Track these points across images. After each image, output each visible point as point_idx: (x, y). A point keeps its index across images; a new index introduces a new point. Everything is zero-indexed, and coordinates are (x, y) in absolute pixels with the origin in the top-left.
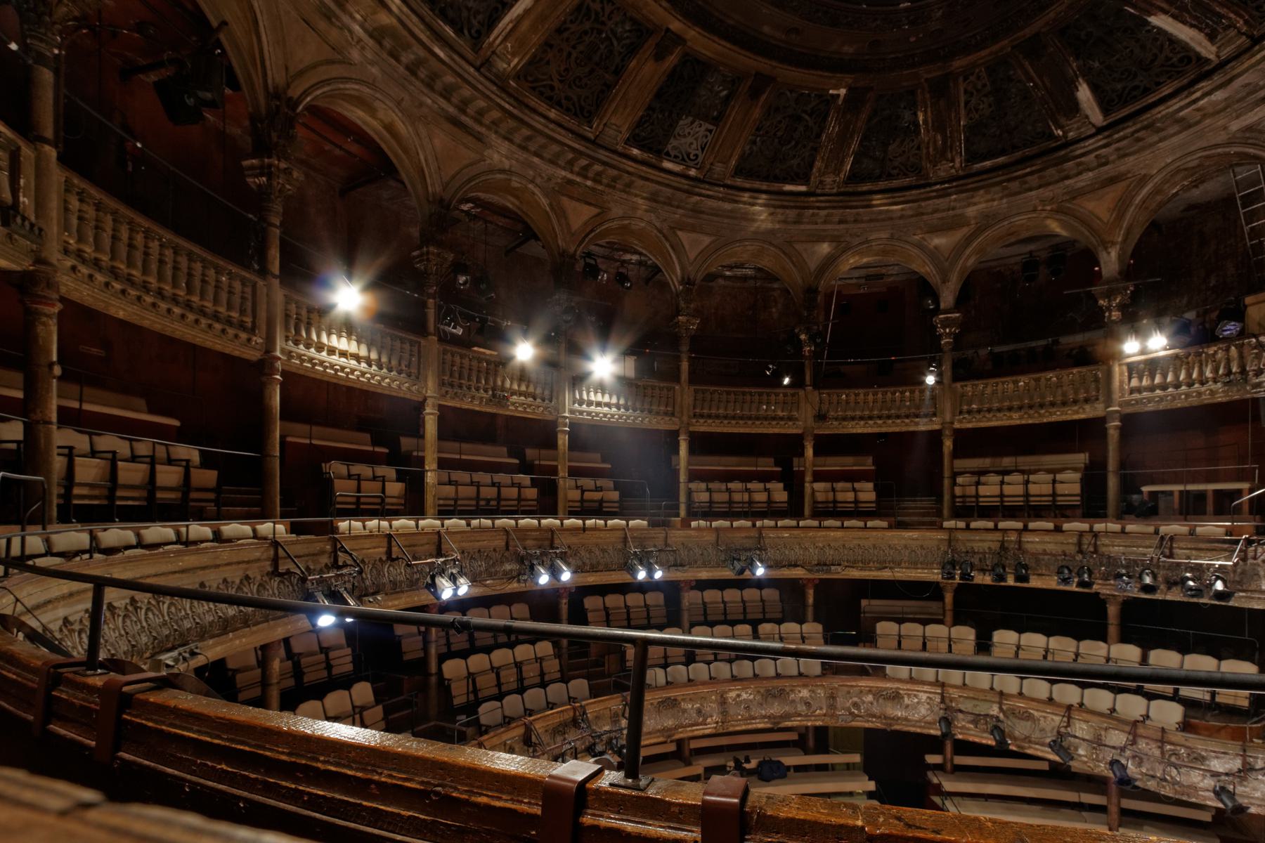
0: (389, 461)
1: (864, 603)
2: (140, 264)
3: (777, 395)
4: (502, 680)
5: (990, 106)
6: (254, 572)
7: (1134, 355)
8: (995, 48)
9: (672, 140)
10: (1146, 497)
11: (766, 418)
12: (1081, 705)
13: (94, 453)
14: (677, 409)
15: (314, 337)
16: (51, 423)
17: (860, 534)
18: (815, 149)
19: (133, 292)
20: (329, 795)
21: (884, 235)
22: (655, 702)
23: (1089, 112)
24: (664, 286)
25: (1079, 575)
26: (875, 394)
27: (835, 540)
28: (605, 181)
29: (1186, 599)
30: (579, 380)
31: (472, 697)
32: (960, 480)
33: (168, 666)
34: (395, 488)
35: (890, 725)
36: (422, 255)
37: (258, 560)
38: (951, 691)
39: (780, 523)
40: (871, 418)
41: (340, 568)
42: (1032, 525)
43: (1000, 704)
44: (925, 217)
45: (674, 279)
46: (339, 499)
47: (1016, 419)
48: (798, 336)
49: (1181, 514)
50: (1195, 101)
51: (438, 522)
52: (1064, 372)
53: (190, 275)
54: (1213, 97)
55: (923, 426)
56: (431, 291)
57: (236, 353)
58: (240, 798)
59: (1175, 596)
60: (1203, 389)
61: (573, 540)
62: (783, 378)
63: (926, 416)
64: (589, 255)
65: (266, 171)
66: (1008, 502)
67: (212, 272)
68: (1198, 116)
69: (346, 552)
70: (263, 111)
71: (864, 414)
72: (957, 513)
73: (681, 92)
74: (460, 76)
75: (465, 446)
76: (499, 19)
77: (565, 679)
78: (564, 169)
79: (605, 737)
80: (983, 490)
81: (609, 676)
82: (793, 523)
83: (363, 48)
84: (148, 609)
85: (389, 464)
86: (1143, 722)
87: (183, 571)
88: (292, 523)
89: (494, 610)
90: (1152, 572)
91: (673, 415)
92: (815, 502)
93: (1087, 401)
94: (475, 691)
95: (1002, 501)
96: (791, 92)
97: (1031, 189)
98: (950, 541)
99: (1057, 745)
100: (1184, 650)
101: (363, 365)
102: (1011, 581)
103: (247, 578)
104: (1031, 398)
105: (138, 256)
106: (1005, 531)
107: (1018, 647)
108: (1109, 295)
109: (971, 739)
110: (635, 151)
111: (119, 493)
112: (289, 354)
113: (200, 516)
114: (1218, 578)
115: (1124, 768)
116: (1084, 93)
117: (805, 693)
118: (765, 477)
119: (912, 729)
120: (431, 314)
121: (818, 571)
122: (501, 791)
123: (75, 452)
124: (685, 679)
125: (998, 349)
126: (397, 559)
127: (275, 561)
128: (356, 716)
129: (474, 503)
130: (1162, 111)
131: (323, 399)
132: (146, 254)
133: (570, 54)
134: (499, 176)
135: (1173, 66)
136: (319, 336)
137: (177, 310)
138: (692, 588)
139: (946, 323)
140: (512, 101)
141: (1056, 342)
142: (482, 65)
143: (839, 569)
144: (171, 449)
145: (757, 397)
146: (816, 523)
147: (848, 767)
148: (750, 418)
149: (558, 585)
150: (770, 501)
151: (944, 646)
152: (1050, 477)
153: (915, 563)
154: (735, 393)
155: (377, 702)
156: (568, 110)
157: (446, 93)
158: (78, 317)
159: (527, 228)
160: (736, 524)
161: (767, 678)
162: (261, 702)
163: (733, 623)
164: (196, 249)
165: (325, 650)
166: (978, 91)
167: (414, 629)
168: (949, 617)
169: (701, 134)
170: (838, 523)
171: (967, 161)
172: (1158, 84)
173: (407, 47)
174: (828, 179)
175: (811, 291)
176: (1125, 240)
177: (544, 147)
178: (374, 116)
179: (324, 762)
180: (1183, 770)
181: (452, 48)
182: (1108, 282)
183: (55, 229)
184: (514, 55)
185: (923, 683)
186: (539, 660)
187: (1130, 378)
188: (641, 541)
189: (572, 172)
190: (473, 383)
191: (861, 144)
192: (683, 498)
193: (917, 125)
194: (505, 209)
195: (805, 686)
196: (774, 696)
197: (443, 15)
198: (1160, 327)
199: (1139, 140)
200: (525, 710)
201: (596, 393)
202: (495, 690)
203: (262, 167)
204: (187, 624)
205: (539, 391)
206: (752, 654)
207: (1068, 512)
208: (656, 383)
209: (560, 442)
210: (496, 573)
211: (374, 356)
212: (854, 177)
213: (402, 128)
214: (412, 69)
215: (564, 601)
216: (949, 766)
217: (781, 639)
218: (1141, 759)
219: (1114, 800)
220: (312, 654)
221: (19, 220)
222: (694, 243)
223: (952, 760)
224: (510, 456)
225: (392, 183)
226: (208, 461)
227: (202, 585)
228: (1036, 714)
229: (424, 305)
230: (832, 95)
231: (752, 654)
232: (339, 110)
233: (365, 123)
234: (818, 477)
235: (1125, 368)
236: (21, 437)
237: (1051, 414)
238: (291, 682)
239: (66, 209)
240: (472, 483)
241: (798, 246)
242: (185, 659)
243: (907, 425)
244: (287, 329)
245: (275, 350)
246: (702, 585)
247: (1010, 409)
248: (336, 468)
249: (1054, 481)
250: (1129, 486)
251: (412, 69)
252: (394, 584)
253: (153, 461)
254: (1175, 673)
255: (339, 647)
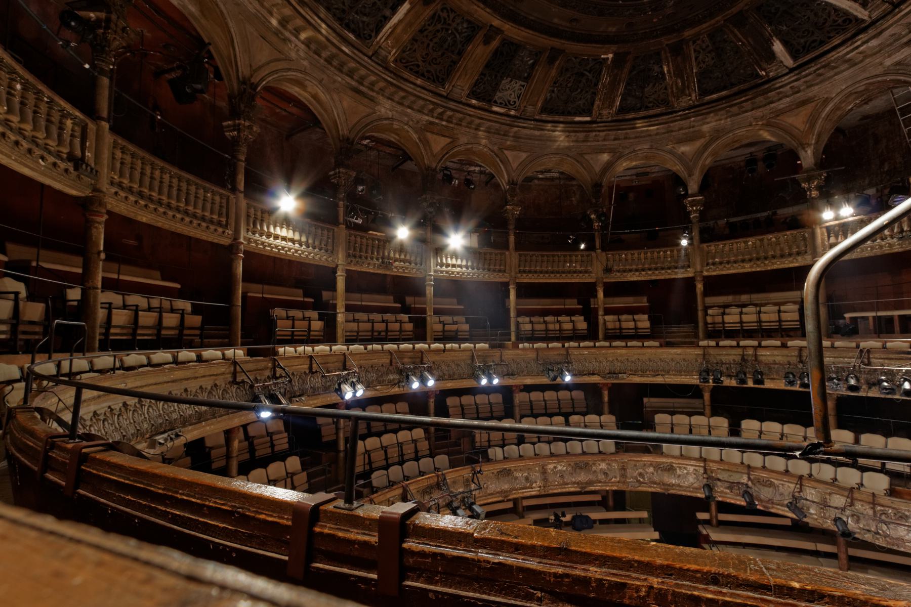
0: (314, 307)
1: (645, 400)
2: (157, 188)
3: (576, 256)
4: (389, 456)
5: (713, 59)
6: (220, 382)
7: (830, 221)
8: (713, 21)
9: (498, 93)
10: (848, 321)
11: (569, 272)
12: (810, 475)
13: (125, 307)
14: (507, 268)
15: (265, 229)
16: (97, 288)
17: (639, 351)
18: (594, 93)
19: (152, 206)
20: (182, 514)
21: (646, 146)
22: (495, 472)
23: (783, 59)
24: (497, 186)
25: (801, 378)
26: (646, 253)
27: (621, 355)
28: (454, 121)
29: (883, 396)
30: (439, 250)
31: (367, 467)
32: (710, 312)
33: (160, 443)
34: (317, 325)
35: (668, 490)
36: (335, 174)
37: (223, 374)
38: (711, 464)
39: (582, 344)
40: (643, 270)
41: (277, 378)
42: (764, 343)
43: (749, 474)
44: (674, 134)
45: (503, 182)
46: (278, 333)
47: (747, 268)
48: (589, 216)
49: (875, 333)
50: (857, 48)
51: (345, 347)
52: (780, 234)
53: (188, 194)
54: (870, 44)
55: (680, 274)
56: (341, 196)
57: (216, 241)
58: (136, 517)
59: (874, 393)
60: (883, 243)
61: (437, 358)
62: (579, 244)
63: (683, 267)
64: (446, 168)
65: (237, 128)
66: (746, 326)
67: (201, 191)
68: (861, 57)
69: (281, 368)
70: (236, 92)
71: (637, 267)
72: (710, 335)
73: (503, 62)
74: (359, 63)
75: (364, 296)
76: (382, 27)
77: (432, 455)
78: (427, 115)
79: (459, 497)
80: (727, 318)
81: (463, 453)
82: (591, 344)
83: (298, 50)
84: (149, 406)
85: (314, 309)
86: (859, 489)
87: (173, 381)
88: (248, 349)
89: (385, 406)
90: (856, 377)
91: (505, 271)
92: (607, 329)
93: (798, 254)
94: (370, 463)
95: (742, 326)
96: (576, 58)
97: (746, 112)
98: (704, 355)
99: (792, 506)
100: (887, 434)
101: (297, 245)
102: (750, 384)
103: (216, 385)
104: (758, 253)
105: (156, 184)
106: (745, 347)
107: (761, 432)
108: (809, 180)
109: (728, 501)
110: (474, 102)
111: (139, 332)
112: (249, 240)
113: (190, 345)
114: (905, 380)
115: (846, 524)
116: (778, 47)
117: (603, 466)
118: (570, 313)
119: (684, 493)
120: (341, 211)
121: (610, 378)
122: (273, 511)
123: (113, 306)
124: (517, 455)
125: (732, 220)
126: (316, 372)
127: (234, 374)
128: (288, 482)
129: (370, 334)
130: (834, 55)
131: (269, 268)
132: (161, 182)
133: (428, 45)
134: (385, 122)
135: (839, 25)
136: (268, 228)
137: (179, 216)
138: (521, 391)
139: (693, 204)
140: (392, 75)
141: (775, 214)
142: (373, 55)
143: (625, 376)
144: (173, 303)
145: (562, 258)
146: (607, 344)
147: (641, 521)
148: (558, 272)
149: (426, 389)
150: (574, 329)
151: (706, 431)
152: (777, 308)
153: (680, 371)
154: (548, 256)
155: (303, 470)
156: (429, 78)
157: (350, 73)
158: (119, 224)
159: (405, 153)
160: (550, 345)
161: (575, 455)
162: (224, 472)
163: (551, 415)
164: (191, 177)
165: (270, 434)
166: (704, 50)
167: (330, 420)
168: (708, 410)
169: (517, 88)
170: (623, 344)
171: (700, 95)
172: (830, 38)
173: (325, 48)
174: (605, 112)
175: (597, 186)
176: (817, 143)
177: (414, 102)
178: (306, 92)
179: (181, 494)
180: (891, 526)
181: (353, 46)
182: (807, 171)
183: (106, 170)
184: (393, 47)
185: (690, 459)
186: (415, 441)
187: (829, 237)
188: (484, 357)
189: (432, 117)
190: (369, 255)
191: (625, 88)
192: (513, 328)
193: (663, 74)
194: (390, 142)
195: (603, 460)
196: (581, 468)
197: (348, 27)
198: (848, 201)
199: (820, 75)
200: (404, 476)
201: (452, 258)
202: (384, 463)
203: (234, 125)
204: (175, 416)
205: (413, 258)
206: (565, 437)
207: (791, 333)
208: (489, 250)
209: (428, 292)
210: (383, 381)
211: (304, 239)
212: (622, 110)
213: (322, 96)
214: (328, 61)
215: (432, 400)
216: (714, 521)
217: (602, 427)
218: (858, 517)
219: (843, 549)
220: (262, 437)
221: (84, 166)
222: (516, 158)
223: (716, 516)
224: (395, 302)
225: (318, 129)
226: (196, 310)
227: (170, 393)
228: (776, 482)
229: (337, 205)
230: (604, 59)
231: (565, 437)
232: (284, 88)
233: (300, 94)
234: (608, 311)
235: (824, 230)
236: (79, 298)
237: (773, 264)
238: (247, 456)
239: (113, 158)
240: (369, 321)
241: (586, 157)
242: (171, 439)
243: (669, 274)
244: (248, 224)
245: (239, 238)
246: (528, 389)
247: (743, 261)
248: (279, 312)
249: (779, 311)
250: (835, 313)
251: (328, 61)
252: (314, 389)
253: (160, 310)
254: (878, 451)
255: (279, 432)
